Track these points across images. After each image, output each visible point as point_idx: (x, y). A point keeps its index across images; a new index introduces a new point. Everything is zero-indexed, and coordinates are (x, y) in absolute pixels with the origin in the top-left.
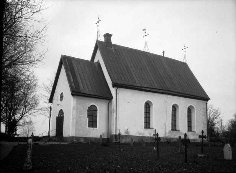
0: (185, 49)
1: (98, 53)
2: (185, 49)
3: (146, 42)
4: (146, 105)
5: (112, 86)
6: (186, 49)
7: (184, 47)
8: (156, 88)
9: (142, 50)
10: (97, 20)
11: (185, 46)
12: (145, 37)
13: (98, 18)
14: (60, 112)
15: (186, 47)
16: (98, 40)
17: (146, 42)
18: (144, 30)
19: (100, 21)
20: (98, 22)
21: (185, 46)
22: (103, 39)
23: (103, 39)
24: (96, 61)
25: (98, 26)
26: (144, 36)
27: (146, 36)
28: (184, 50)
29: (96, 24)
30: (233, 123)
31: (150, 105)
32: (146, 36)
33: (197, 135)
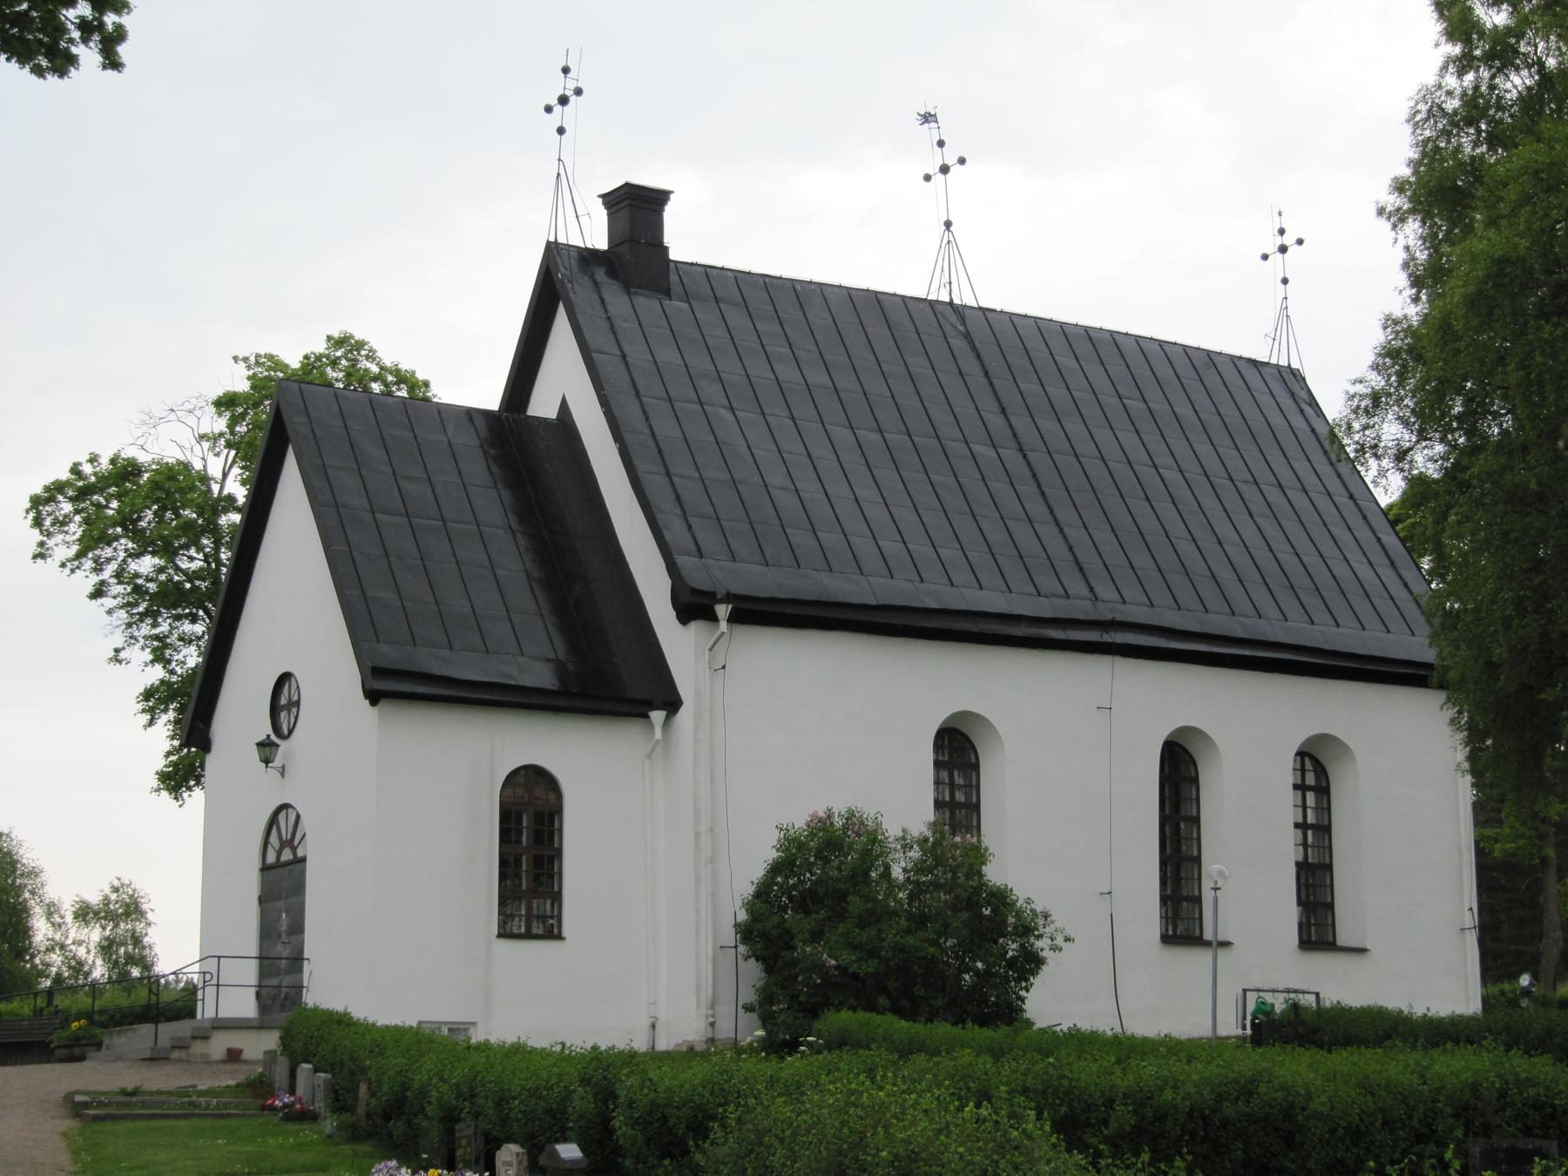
0: (1283, 249)
1: (562, 340)
2: (1283, 249)
3: (948, 224)
4: (1303, 770)
5: (671, 614)
6: (1293, 250)
7: (1279, 241)
8: (1108, 616)
9: (920, 293)
10: (558, 86)
11: (1282, 232)
12: (940, 177)
13: (566, 70)
14: (273, 821)
15: (1289, 239)
16: (562, 240)
17: (948, 224)
18: (928, 118)
19: (578, 92)
20: (563, 100)
21: (1282, 232)
22: (595, 233)
23: (595, 233)
24: (543, 405)
25: (561, 131)
26: (933, 169)
27: (945, 169)
28: (951, 160)
29: (549, 109)
30: (346, 1043)
31: (1325, 764)
32: (945, 169)
33: (1182, 1055)
